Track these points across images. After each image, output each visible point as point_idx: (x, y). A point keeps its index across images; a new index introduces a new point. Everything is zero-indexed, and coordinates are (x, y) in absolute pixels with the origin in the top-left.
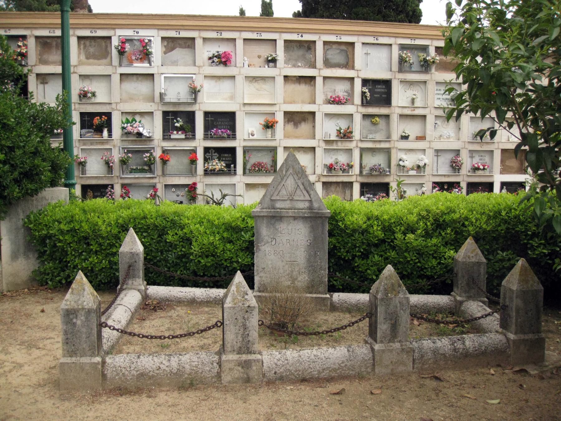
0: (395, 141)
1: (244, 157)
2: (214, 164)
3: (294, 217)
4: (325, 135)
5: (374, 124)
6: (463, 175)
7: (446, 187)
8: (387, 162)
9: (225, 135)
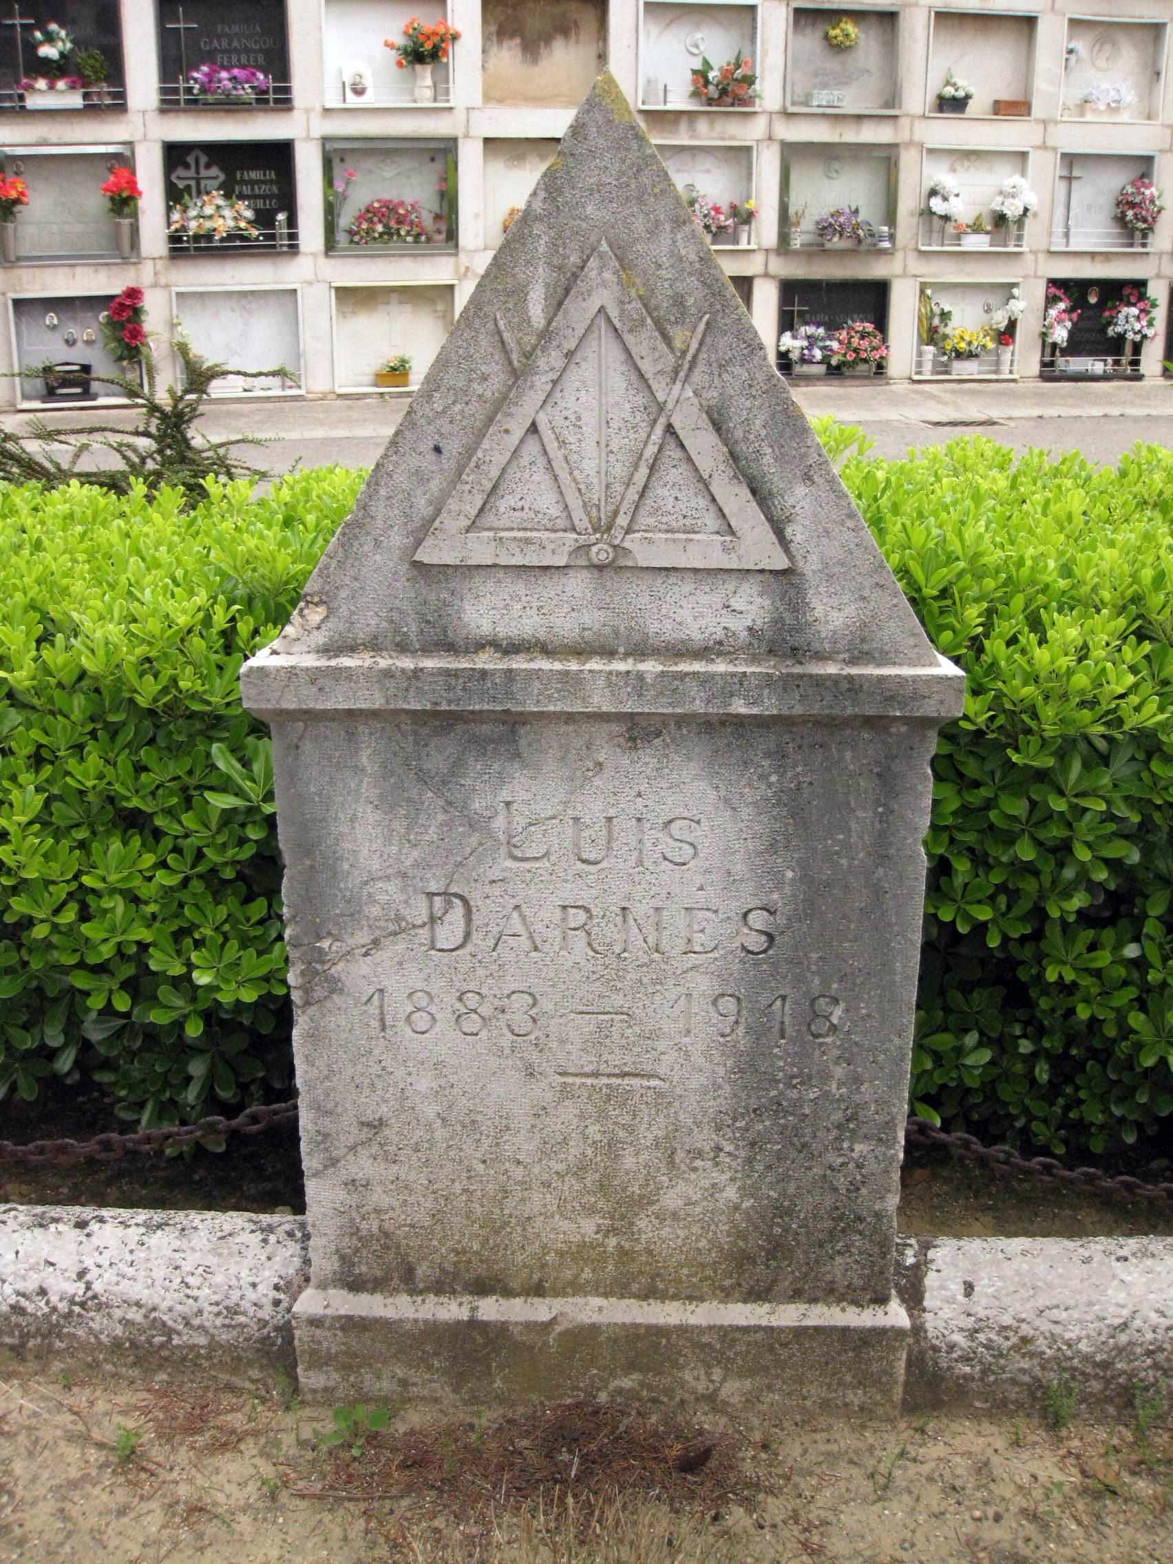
0: (913, 117)
1: (329, 180)
2: (209, 210)
3: (631, 719)
4: (646, 92)
5: (838, 48)
6: (1160, 255)
7: (1093, 300)
8: (880, 201)
9: (246, 92)
